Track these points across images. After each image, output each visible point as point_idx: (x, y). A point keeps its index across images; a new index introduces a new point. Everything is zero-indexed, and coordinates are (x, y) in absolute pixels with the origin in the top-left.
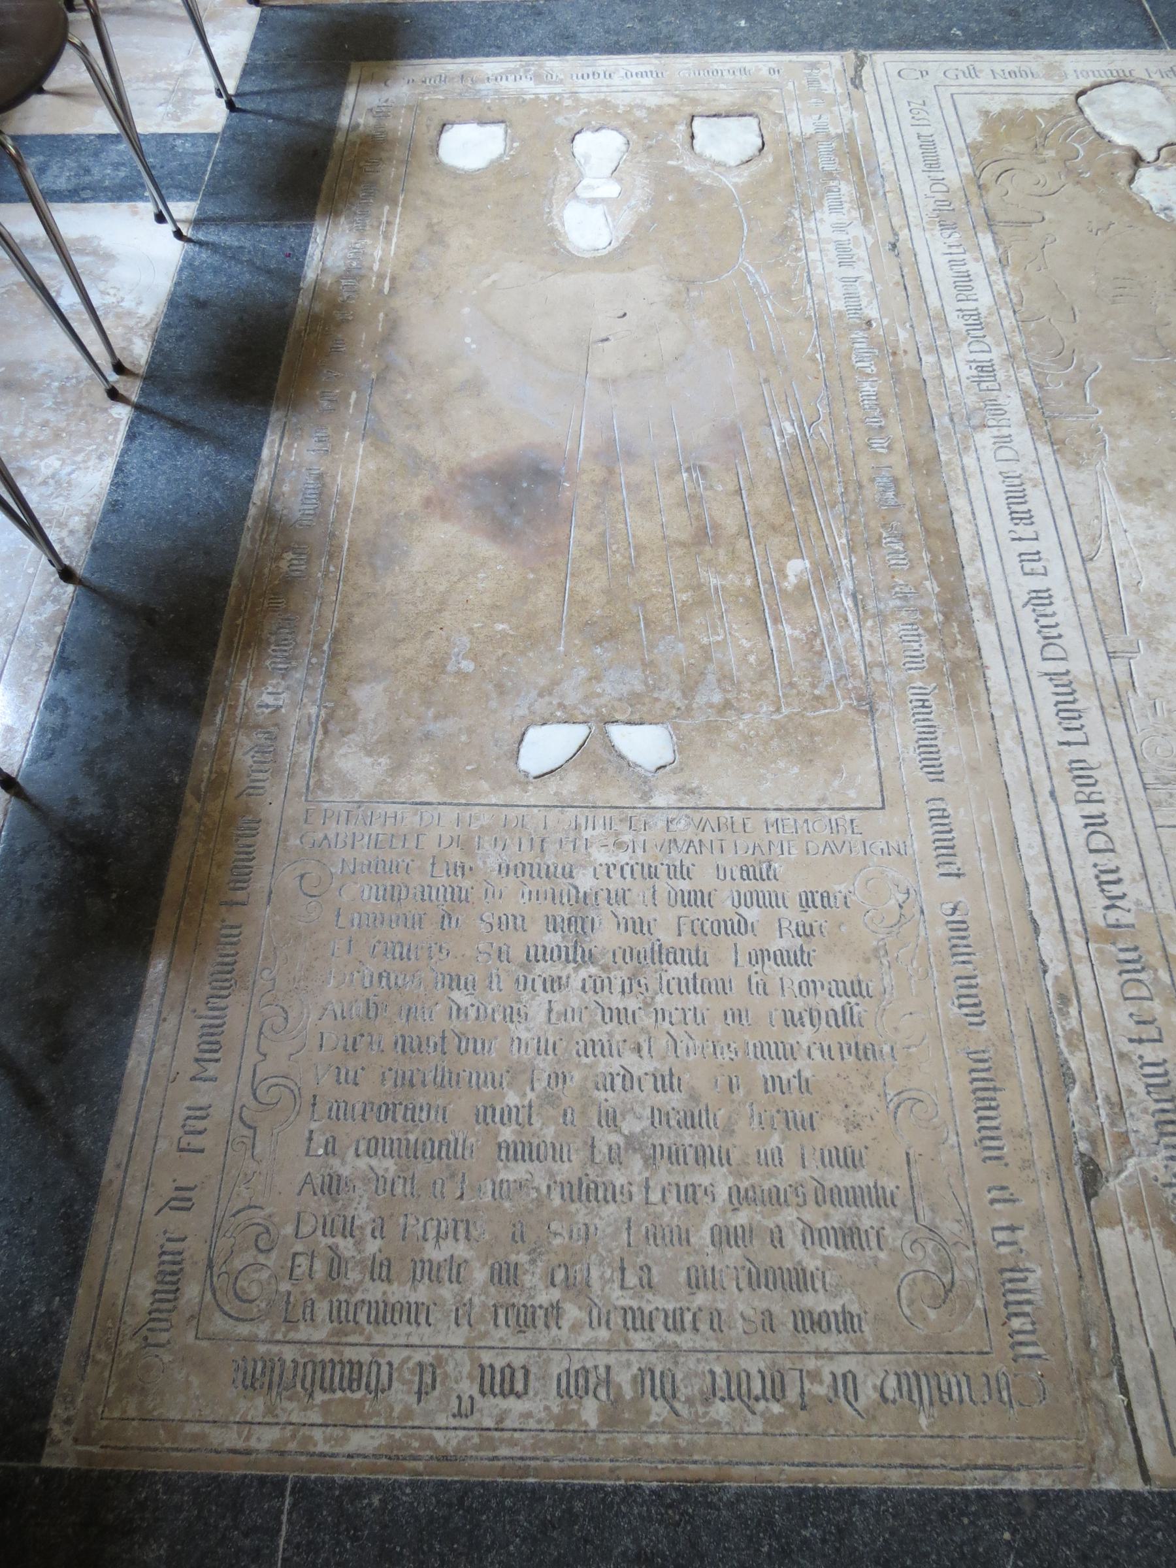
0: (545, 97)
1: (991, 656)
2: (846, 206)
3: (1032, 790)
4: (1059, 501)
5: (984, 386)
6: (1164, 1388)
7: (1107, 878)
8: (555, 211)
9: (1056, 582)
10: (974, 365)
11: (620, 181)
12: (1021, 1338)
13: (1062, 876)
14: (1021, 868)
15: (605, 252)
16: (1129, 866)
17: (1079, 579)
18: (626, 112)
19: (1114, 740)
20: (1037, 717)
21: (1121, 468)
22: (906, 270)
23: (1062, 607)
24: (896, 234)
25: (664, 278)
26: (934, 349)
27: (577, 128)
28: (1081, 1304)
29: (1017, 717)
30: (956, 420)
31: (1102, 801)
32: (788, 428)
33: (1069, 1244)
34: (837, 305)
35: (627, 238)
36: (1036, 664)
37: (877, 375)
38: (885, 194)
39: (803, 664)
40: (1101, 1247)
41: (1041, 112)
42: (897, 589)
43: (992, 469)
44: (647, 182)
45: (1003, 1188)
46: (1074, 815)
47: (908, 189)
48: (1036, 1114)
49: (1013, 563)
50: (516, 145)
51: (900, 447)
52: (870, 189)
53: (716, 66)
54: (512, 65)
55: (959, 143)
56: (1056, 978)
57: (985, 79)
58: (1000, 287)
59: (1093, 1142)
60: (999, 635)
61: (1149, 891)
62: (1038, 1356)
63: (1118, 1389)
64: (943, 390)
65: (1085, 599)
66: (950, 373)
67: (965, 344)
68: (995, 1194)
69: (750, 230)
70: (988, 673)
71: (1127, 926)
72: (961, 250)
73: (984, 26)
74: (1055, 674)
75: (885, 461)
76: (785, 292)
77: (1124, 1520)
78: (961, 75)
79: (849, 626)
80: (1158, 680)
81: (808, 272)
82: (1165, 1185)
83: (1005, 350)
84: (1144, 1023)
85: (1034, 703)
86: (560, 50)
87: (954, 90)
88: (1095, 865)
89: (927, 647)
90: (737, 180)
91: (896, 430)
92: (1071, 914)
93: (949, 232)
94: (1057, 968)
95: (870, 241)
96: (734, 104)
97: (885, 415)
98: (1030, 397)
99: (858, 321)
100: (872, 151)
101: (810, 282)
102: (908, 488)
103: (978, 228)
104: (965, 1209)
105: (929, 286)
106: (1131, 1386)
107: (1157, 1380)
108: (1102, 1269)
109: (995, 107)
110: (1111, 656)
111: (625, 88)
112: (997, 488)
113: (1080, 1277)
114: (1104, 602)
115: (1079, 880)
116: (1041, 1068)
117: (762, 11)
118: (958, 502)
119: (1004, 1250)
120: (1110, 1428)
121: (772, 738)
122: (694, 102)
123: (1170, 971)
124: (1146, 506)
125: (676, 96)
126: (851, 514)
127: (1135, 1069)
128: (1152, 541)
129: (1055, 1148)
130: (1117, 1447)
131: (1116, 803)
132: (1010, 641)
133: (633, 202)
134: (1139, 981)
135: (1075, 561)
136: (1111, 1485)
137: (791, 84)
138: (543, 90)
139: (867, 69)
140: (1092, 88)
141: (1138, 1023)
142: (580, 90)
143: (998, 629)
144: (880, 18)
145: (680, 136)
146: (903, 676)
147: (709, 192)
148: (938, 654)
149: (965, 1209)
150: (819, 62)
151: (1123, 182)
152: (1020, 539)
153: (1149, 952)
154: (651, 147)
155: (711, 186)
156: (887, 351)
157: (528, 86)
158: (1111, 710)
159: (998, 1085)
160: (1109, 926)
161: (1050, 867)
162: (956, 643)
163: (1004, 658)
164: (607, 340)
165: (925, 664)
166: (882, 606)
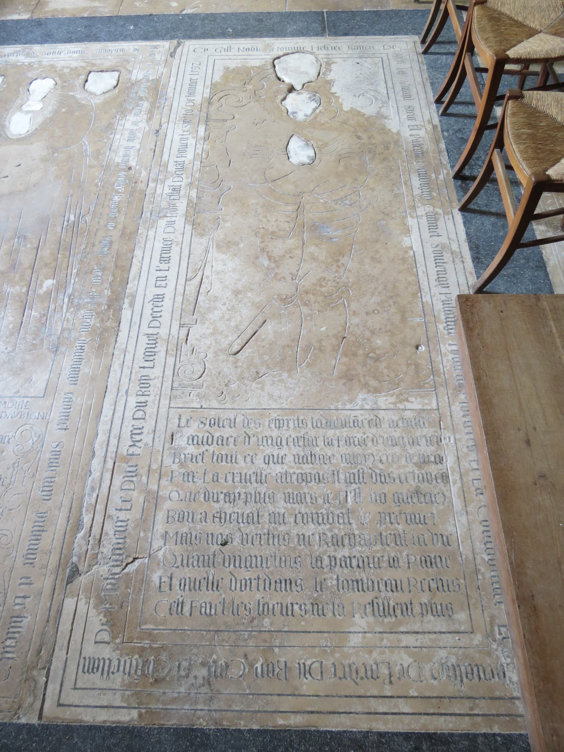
0: (27, 64)
1: (124, 326)
2: (142, 113)
3: (118, 389)
4: (186, 252)
5: (172, 198)
6: (66, 675)
7: (137, 432)
8: (8, 117)
9: (169, 292)
10: (171, 188)
11: (43, 103)
12: (8, 649)
13: (116, 430)
14: (97, 426)
15: (24, 136)
16: (149, 425)
17: (180, 289)
18: (60, 70)
19: (166, 366)
20: (134, 355)
21: (221, 237)
22: (158, 143)
23: (167, 303)
24: (160, 125)
25: (45, 148)
26: (156, 181)
27: (35, 77)
28: (43, 634)
29: (125, 354)
30: (153, 214)
31: (149, 395)
32: (72, 218)
33: (49, 605)
34: (118, 160)
35: (36, 129)
36: (145, 329)
37: (123, 193)
38: (164, 107)
39: (33, 329)
40: (64, 607)
41: (252, 68)
42: (91, 294)
43: (161, 235)
44: (56, 103)
45: (28, 578)
46: (132, 401)
47: (175, 104)
48: (57, 543)
49: (152, 281)
50: (4, 86)
51: (120, 227)
52: (158, 105)
53: (110, 48)
54: (18, 49)
55: (208, 83)
56: (93, 479)
57: (234, 51)
58: (199, 151)
59: (80, 558)
60: (132, 316)
61: (154, 438)
62: (13, 658)
63: (45, 675)
64: (152, 200)
65: (179, 299)
66: (159, 191)
67: (172, 178)
68: (23, 580)
69: (94, 125)
70: (120, 334)
71: (137, 455)
72: (188, 133)
73: (244, 27)
74: (151, 334)
75: (110, 233)
76: (98, 154)
77: (21, 737)
78: (223, 50)
79: (62, 311)
80: (199, 338)
81: (111, 145)
82: (104, 579)
83: (189, 181)
84: (126, 501)
85: (136, 348)
86: (42, 41)
87: (216, 58)
88: (133, 426)
89: (93, 321)
90: (97, 101)
91: (122, 219)
92: (112, 449)
93: (186, 124)
94: (96, 474)
95: (147, 129)
96: (111, 66)
97: (119, 212)
98: (192, 202)
99: (125, 167)
100: (166, 86)
101: (110, 149)
102: (115, 247)
103: (201, 123)
104: (6, 587)
105: (166, 151)
106: (51, 674)
107: (64, 671)
108: (60, 618)
109: (232, 65)
110: (181, 326)
111: (64, 59)
112: (159, 246)
113: (48, 621)
114: (188, 300)
115: (122, 432)
116: (69, 521)
117: (143, 22)
118: (138, 253)
119: (17, 607)
120: (34, 694)
121: (5, 363)
122: (93, 65)
123: (148, 477)
124: (226, 255)
125: (86, 62)
126: (84, 258)
127: (113, 523)
128: (222, 271)
129: (60, 560)
130: (34, 702)
131: (155, 396)
132: (136, 319)
133: (46, 112)
134: (132, 481)
135: (182, 281)
136: (23, 721)
137: (141, 56)
138: (27, 61)
139: (180, 48)
140: (284, 55)
141: (123, 501)
142: (44, 60)
143: (132, 313)
144: (197, 24)
145: (80, 81)
146: (77, 335)
147: (82, 107)
148: (98, 325)
149: (6, 587)
150: (158, 45)
151: (278, 101)
152: (160, 270)
153: (142, 468)
154: (64, 86)
155: (84, 104)
156: (132, 181)
157: (22, 59)
158: (171, 352)
159: (45, 529)
160: (128, 455)
161: (111, 426)
162: (109, 319)
163: (130, 327)
164: (7, 177)
165: (90, 329)
166: (80, 302)
